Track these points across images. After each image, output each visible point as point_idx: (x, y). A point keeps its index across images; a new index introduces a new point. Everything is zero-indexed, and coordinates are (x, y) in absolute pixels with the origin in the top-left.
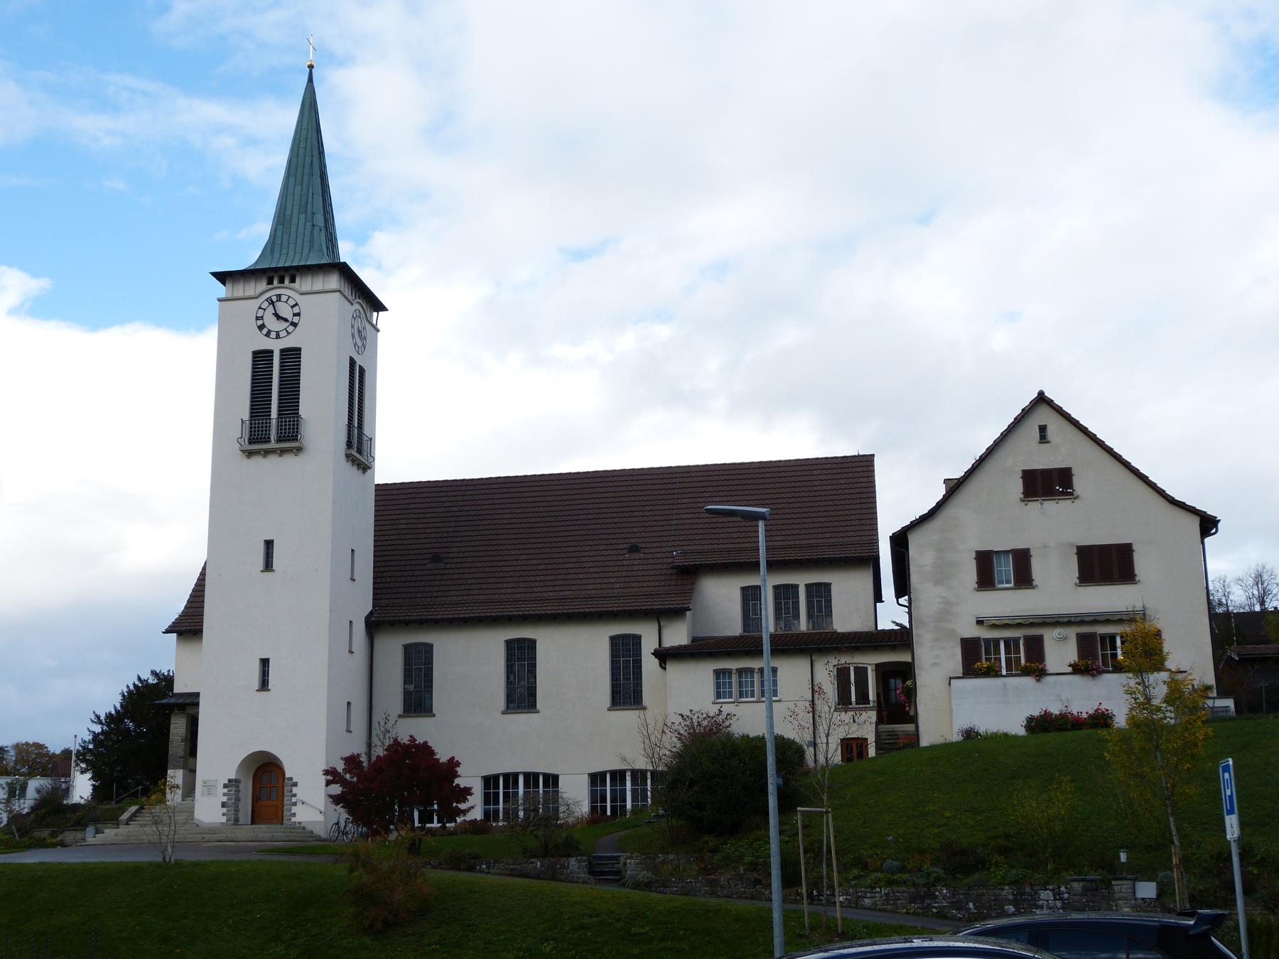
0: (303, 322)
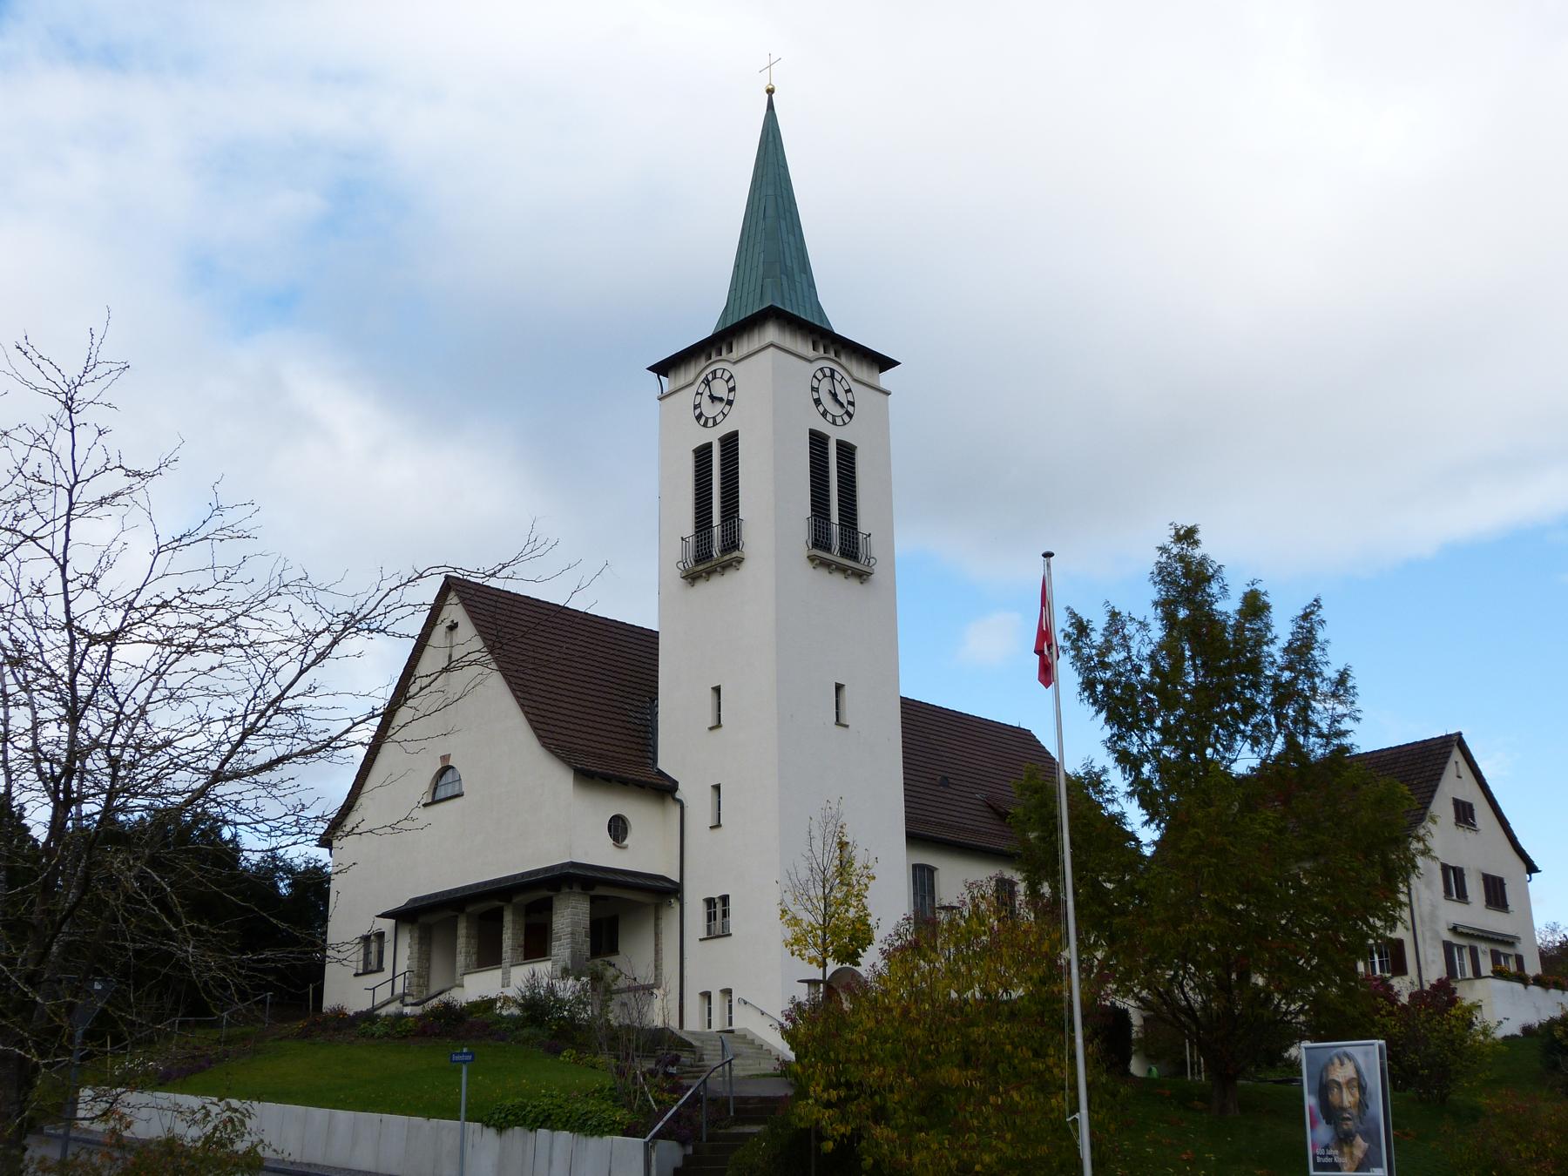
0: (738, 398)
